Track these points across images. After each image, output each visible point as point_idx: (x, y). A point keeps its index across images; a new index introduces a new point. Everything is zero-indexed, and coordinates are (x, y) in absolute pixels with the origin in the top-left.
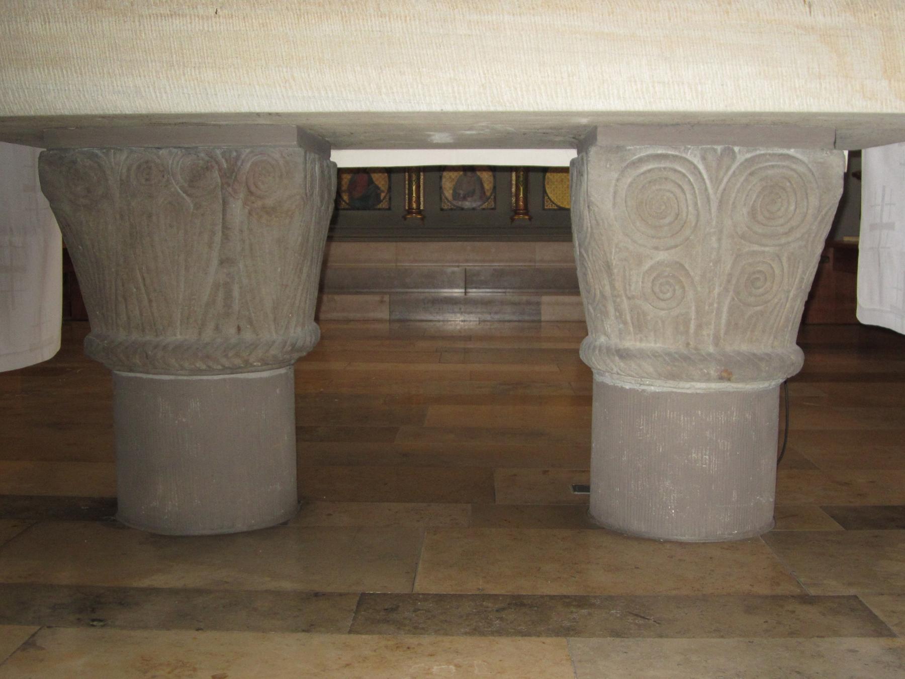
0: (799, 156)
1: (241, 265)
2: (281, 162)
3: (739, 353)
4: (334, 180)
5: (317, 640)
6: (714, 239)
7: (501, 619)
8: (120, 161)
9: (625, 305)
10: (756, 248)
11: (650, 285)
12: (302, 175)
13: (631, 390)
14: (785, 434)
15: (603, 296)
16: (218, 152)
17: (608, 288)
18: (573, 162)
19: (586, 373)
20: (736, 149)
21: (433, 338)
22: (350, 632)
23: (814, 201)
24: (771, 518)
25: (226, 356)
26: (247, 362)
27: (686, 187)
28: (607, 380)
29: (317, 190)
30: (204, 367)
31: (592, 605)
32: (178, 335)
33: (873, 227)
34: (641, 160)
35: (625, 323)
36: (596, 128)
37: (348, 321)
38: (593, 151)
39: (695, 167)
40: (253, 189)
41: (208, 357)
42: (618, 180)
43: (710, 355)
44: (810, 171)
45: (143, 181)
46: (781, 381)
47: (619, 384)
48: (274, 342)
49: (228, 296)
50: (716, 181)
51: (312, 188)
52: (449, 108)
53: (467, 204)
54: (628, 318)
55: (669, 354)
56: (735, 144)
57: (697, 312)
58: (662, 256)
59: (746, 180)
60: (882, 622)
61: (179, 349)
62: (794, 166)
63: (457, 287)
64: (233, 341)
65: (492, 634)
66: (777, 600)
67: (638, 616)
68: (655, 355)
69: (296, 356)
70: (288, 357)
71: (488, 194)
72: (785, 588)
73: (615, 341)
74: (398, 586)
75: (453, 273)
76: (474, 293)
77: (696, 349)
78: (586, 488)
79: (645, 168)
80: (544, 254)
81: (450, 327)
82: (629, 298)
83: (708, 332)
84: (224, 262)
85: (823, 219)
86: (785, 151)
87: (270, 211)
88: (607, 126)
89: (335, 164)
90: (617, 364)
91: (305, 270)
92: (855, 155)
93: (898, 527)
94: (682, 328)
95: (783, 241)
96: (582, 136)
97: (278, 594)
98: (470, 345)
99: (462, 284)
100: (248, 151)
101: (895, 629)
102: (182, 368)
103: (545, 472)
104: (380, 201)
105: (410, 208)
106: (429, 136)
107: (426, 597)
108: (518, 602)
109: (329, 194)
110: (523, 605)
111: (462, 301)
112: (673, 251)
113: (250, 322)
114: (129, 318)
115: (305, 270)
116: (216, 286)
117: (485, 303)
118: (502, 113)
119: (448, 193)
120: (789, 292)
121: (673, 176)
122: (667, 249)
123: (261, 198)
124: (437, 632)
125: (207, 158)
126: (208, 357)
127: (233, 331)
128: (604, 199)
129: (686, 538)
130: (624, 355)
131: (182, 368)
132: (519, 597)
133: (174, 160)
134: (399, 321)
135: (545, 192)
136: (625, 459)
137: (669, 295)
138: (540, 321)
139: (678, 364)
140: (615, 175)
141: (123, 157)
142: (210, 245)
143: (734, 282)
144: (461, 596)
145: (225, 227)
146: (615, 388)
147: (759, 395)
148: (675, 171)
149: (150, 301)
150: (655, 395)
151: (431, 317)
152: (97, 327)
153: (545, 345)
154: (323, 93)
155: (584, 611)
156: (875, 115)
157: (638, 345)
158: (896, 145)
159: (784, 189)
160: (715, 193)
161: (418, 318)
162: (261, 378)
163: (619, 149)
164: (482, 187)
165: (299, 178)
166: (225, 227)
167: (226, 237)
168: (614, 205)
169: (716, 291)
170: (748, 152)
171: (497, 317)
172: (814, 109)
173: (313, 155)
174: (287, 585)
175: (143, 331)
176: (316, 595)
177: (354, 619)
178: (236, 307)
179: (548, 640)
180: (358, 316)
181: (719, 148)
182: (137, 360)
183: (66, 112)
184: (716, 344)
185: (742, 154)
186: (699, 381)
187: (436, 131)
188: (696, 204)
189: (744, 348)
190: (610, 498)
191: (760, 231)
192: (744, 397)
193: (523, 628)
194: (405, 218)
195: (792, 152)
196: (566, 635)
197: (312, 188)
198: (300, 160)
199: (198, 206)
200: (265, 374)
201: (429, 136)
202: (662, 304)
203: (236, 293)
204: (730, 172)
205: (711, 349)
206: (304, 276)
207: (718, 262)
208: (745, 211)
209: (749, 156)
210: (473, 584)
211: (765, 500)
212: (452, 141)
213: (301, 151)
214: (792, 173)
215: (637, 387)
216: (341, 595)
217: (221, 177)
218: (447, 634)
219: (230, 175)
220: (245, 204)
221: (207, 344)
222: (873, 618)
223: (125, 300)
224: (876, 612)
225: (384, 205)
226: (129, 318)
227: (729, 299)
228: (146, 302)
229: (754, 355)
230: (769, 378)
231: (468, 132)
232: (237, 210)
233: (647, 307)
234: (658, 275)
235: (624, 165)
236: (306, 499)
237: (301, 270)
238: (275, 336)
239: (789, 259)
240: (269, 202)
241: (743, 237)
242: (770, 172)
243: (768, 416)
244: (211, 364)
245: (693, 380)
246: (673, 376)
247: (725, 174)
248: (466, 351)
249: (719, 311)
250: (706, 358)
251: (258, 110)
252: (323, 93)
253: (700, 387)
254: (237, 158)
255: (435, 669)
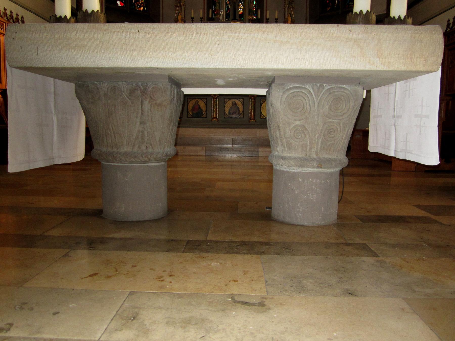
0: (347, 87)
1: (148, 124)
2: (162, 88)
3: (325, 158)
4: (182, 99)
5: (171, 254)
6: (316, 117)
7: (238, 249)
8: (104, 86)
9: (284, 140)
10: (331, 120)
11: (293, 133)
12: (170, 92)
13: (286, 171)
14: (342, 194)
15: (277, 138)
16: (140, 83)
17: (278, 134)
18: (267, 92)
19: (271, 167)
20: (324, 85)
21: (220, 161)
22: (183, 252)
23: (352, 104)
24: (336, 219)
25: (142, 157)
26: (149, 159)
27: (306, 98)
28: (278, 168)
29: (175, 99)
30: (134, 161)
31: (270, 245)
32: (125, 149)
33: (375, 117)
34: (290, 89)
35: (284, 147)
36: (275, 77)
37: (190, 156)
38: (273, 85)
39: (310, 91)
40: (152, 96)
41: (135, 157)
42: (282, 95)
43: (314, 158)
44: (351, 93)
45: (113, 93)
46: (340, 169)
47: (282, 169)
48: (159, 153)
49: (143, 136)
50: (317, 96)
51: (174, 97)
52: (221, 67)
53: (234, 116)
54: (285, 145)
55: (300, 158)
56: (325, 83)
57: (310, 143)
58: (298, 123)
59: (328, 96)
60: (375, 252)
61: (126, 154)
62: (345, 91)
63: (230, 144)
64: (145, 151)
65: (234, 253)
66: (338, 244)
67: (287, 249)
68: (295, 158)
69: (168, 158)
70: (164, 158)
71: (241, 113)
72: (341, 241)
73: (280, 154)
74: (201, 237)
75: (228, 139)
76: (235, 146)
77: (309, 156)
78: (271, 208)
79: (292, 91)
80: (260, 133)
81: (226, 158)
82: (286, 138)
83: (314, 150)
84: (142, 123)
85: (355, 110)
86: (342, 86)
87: (158, 105)
88: (279, 77)
89: (183, 92)
90: (281, 162)
91: (171, 127)
92: (368, 92)
93: (382, 222)
94: (304, 149)
95: (341, 118)
96: (269, 80)
97: (158, 240)
98: (234, 164)
99: (231, 143)
100: (151, 83)
101: (379, 254)
102: (126, 161)
103: (257, 203)
104: (203, 115)
105: (213, 117)
106: (216, 81)
107: (211, 241)
108: (243, 243)
109: (180, 101)
110: (245, 244)
111: (232, 148)
112: (302, 121)
113: (151, 145)
114: (107, 143)
115: (171, 127)
116: (139, 132)
117: (239, 150)
118: (241, 69)
119: (227, 112)
120: (343, 136)
121: (301, 94)
122: (299, 120)
123: (155, 100)
124: (214, 252)
125: (135, 86)
126: (135, 157)
127: (144, 148)
128: (279, 106)
129: (306, 224)
130: (284, 158)
131: (126, 161)
132: (245, 242)
133: (124, 86)
134: (208, 156)
135: (261, 112)
136: (284, 196)
137: (300, 137)
138: (258, 157)
139: (303, 162)
140: (281, 94)
141: (106, 85)
142: (137, 117)
143: (323, 132)
144: (224, 241)
145: (142, 111)
146: (280, 171)
147: (332, 174)
148: (303, 92)
149: (115, 137)
150: (295, 173)
151: (220, 155)
152: (96, 146)
153: (260, 164)
154: (176, 61)
155: (267, 247)
156: (374, 71)
157: (289, 155)
158: (383, 87)
159: (341, 99)
160: (317, 101)
161: (215, 155)
162: (155, 166)
163: (283, 84)
164: (239, 110)
165: (169, 93)
166: (142, 111)
167: (142, 114)
168: (281, 104)
169: (317, 135)
170: (329, 86)
171: (243, 155)
172: (352, 68)
173: (174, 86)
174: (162, 237)
175: (112, 147)
176: (172, 240)
177: (185, 248)
178: (146, 140)
179: (254, 256)
180: (194, 154)
181: (318, 85)
182: (110, 158)
183: (84, 66)
184: (317, 155)
185: (326, 87)
186: (310, 168)
187: (218, 78)
188: (310, 104)
189: (327, 156)
190: (279, 211)
191: (333, 114)
192: (327, 174)
193: (245, 252)
194: (211, 121)
195: (344, 86)
196: (260, 254)
197: (174, 97)
198: (169, 87)
199: (132, 103)
200: (156, 164)
201: (216, 81)
202: (297, 140)
203: (146, 134)
204: (322, 94)
205: (315, 157)
206: (171, 129)
207: (317, 125)
208: (327, 107)
209: (329, 87)
210: (229, 238)
211: (334, 211)
212: (224, 84)
213: (170, 84)
214: (344, 94)
215: (288, 170)
216: (180, 240)
217: (141, 92)
218: (217, 253)
219: (144, 92)
220: (149, 102)
221: (135, 153)
222: (372, 251)
223: (106, 136)
224: (373, 249)
225: (204, 116)
226: (107, 143)
227: (321, 139)
228: (113, 137)
229: (330, 159)
230: (336, 167)
231: (230, 79)
232: (147, 105)
233: (292, 141)
234: (296, 130)
235: (284, 90)
236: (170, 211)
237: (169, 127)
238: (160, 151)
239: (343, 124)
240: (158, 102)
241: (326, 116)
242: (336, 93)
243: (336, 180)
244: (136, 160)
245: (308, 167)
246: (301, 166)
247: (320, 94)
248: (232, 165)
249: (318, 142)
250: (313, 160)
251: (153, 67)
252: (176, 61)
253: (311, 170)
254: (147, 86)
255: (213, 264)
